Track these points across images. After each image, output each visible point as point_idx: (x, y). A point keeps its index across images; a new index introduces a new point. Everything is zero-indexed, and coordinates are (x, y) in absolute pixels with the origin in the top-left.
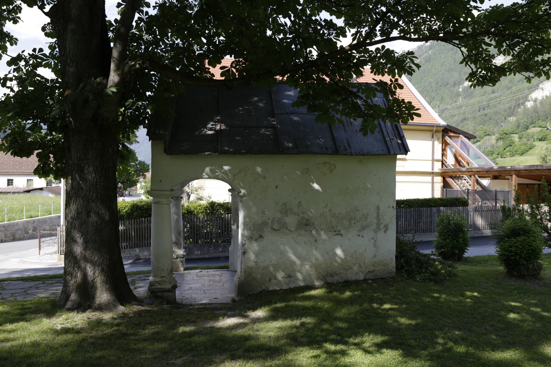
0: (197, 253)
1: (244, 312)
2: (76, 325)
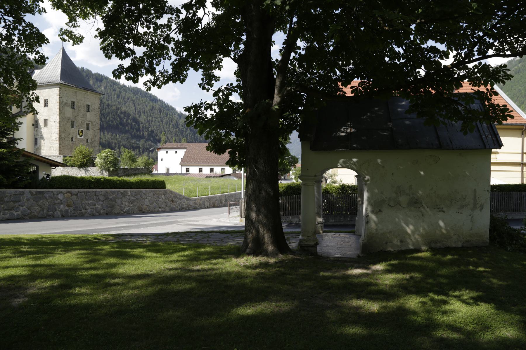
0: (332, 221)
1: (367, 265)
2: (252, 264)
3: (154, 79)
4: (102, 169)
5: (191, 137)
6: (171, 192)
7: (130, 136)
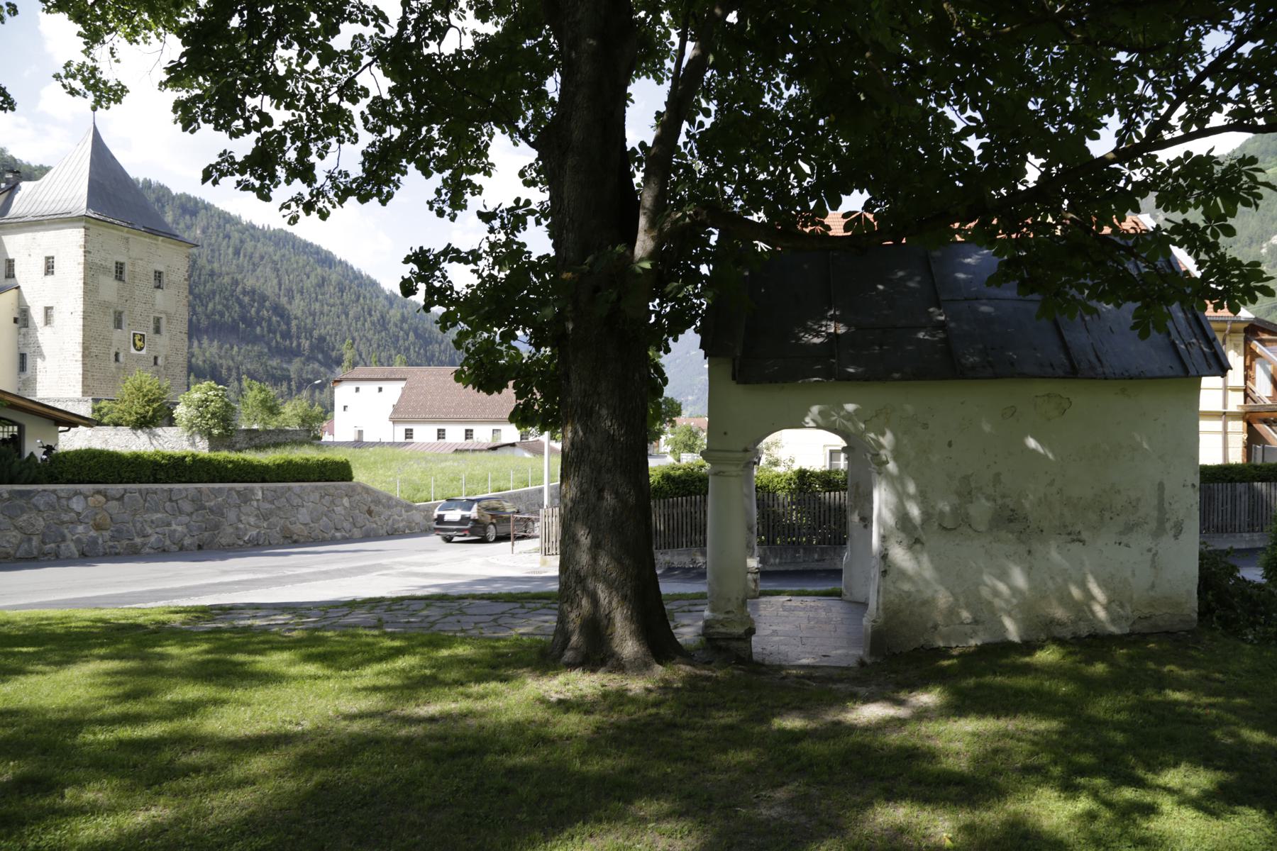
0: (775, 563)
4: (193, 433)
5: (419, 353)
6: (367, 490)
7: (266, 350)
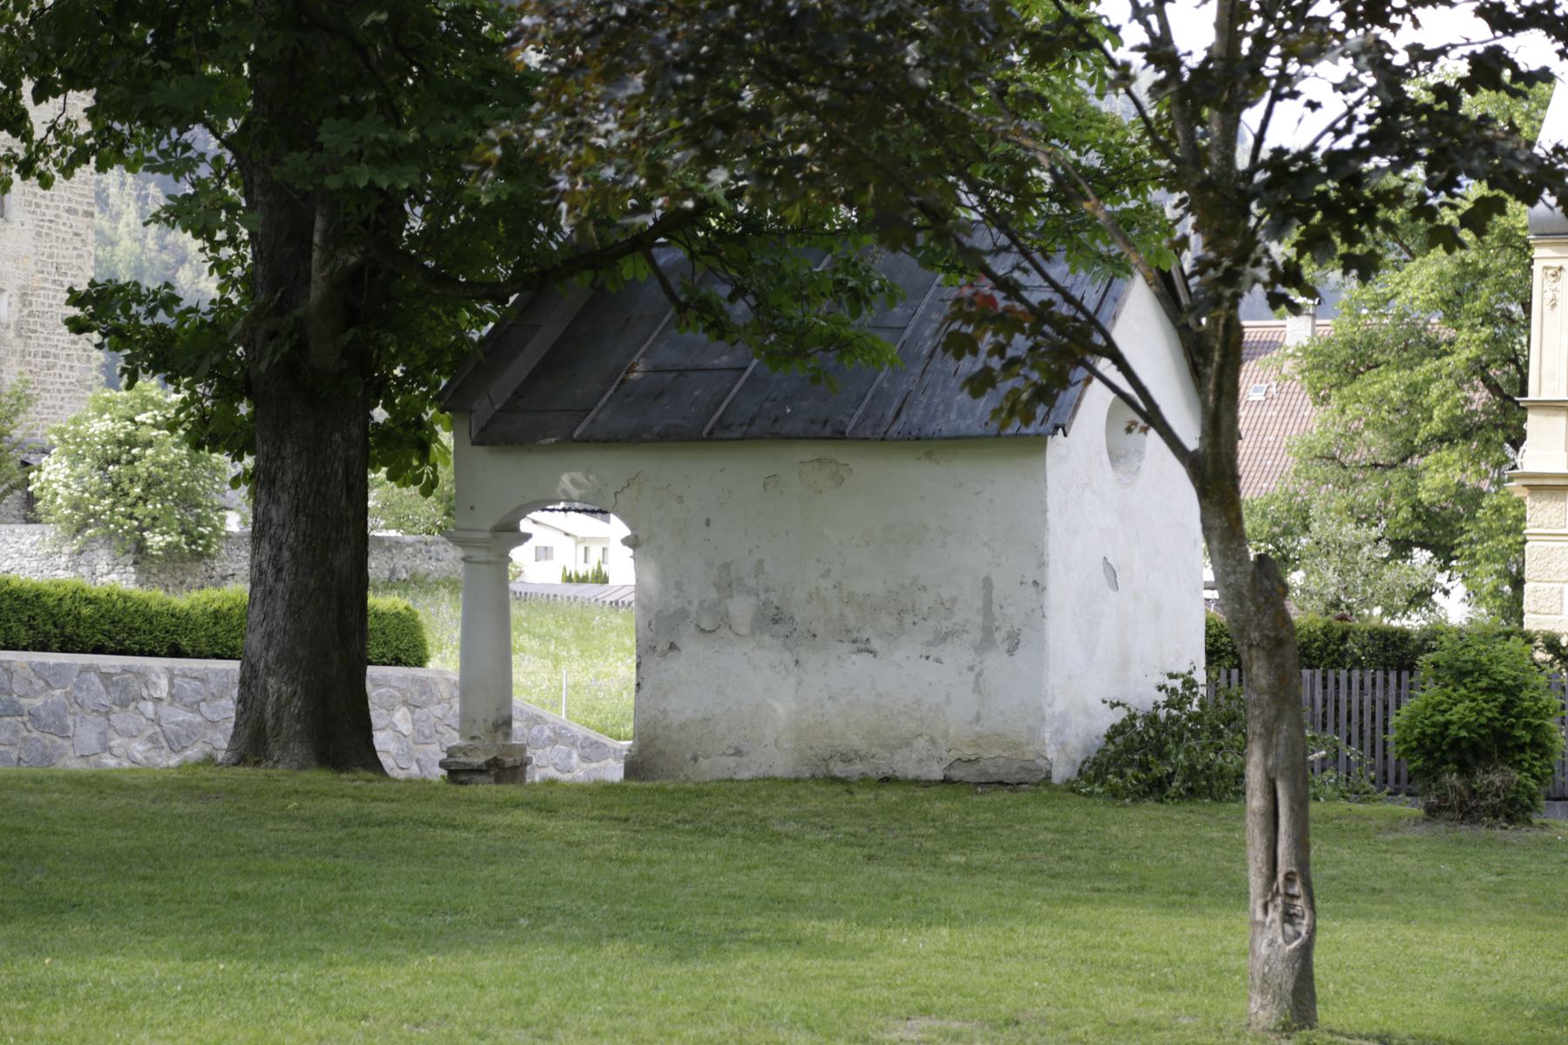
3: (27, 149)
